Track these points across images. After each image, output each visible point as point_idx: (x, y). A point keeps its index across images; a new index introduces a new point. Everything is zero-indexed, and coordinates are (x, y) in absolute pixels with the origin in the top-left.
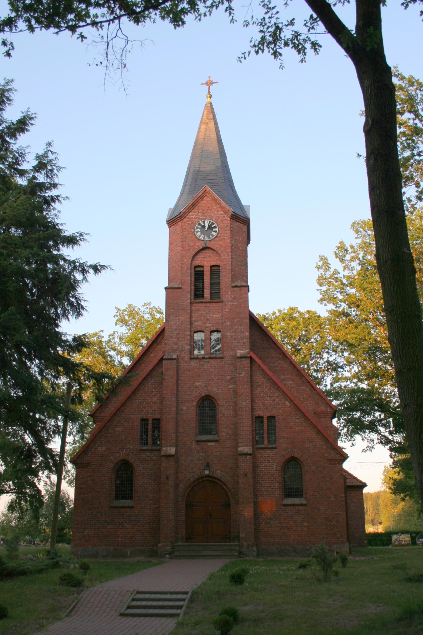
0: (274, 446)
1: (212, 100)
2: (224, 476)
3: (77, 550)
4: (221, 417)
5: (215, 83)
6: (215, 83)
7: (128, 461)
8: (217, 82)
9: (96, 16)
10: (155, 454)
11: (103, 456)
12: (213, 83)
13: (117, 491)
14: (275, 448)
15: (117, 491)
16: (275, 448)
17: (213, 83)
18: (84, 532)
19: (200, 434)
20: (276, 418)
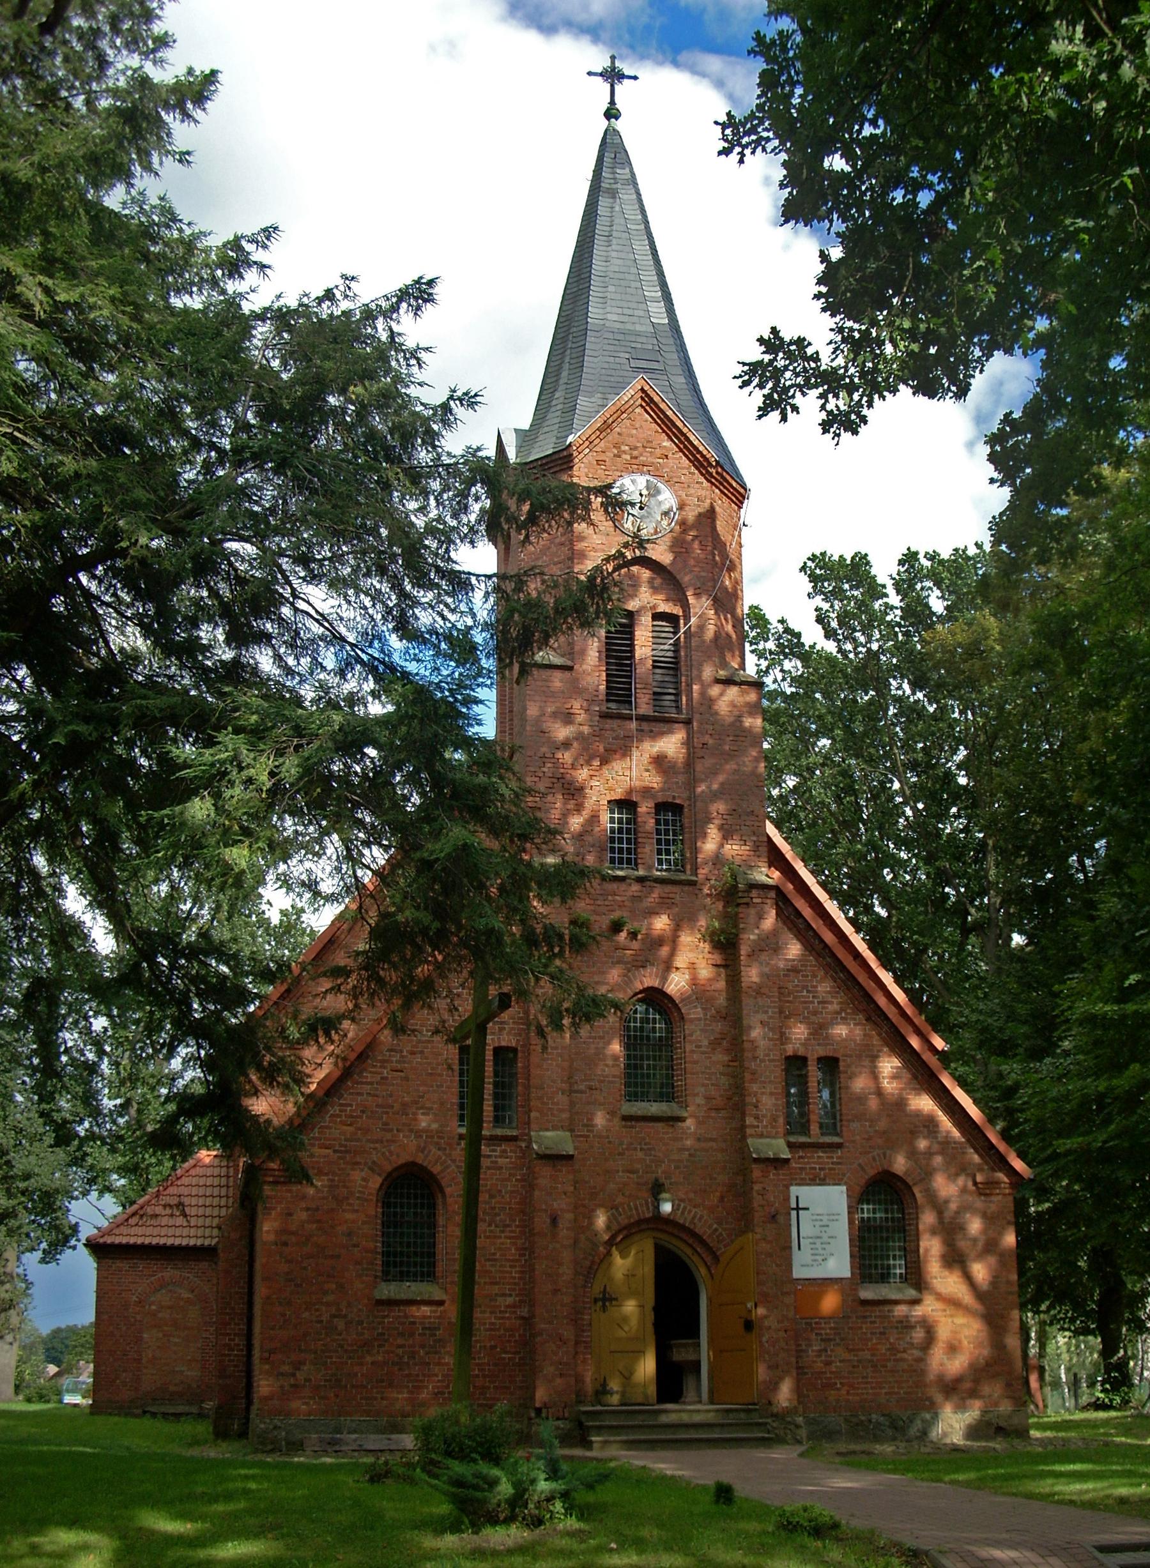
0: (836, 1140)
1: (619, 125)
2: (701, 1217)
3: (275, 1427)
4: (692, 1051)
5: (595, 74)
6: (595, 74)
7: (422, 1168)
8: (590, 74)
9: (337, 989)
10: (504, 1151)
11: (346, 1152)
12: (601, 75)
13: (389, 1207)
14: (839, 1146)
15: (389, 1207)
16: (839, 1146)
17: (601, 75)
18: (294, 1375)
19: (632, 1097)
20: (841, 1064)
